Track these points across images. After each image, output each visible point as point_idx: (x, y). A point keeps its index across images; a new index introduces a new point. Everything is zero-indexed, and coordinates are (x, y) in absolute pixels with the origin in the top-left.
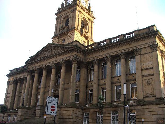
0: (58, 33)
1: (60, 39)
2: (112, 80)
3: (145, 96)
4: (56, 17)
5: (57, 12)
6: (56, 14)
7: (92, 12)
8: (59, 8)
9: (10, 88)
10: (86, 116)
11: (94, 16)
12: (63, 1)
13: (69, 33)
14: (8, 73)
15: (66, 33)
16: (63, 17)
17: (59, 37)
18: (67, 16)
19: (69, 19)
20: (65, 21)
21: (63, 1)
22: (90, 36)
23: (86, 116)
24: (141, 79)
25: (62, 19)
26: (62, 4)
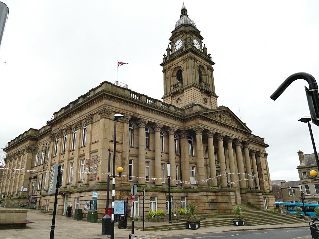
0: (169, 91)
1: (173, 99)
2: (169, 157)
3: (90, 178)
4: (162, 68)
5: (162, 62)
6: (162, 65)
7: (209, 55)
8: (165, 55)
9: (265, 165)
10: (77, 203)
11: (213, 60)
12: (168, 45)
13: (184, 91)
14: (5, 145)
15: (181, 91)
16: (173, 67)
17: (171, 97)
18: (179, 67)
19: (181, 71)
20: (175, 74)
21: (168, 45)
22: (211, 90)
23: (77, 203)
24: (68, 153)
25: (172, 71)
26: (168, 50)
